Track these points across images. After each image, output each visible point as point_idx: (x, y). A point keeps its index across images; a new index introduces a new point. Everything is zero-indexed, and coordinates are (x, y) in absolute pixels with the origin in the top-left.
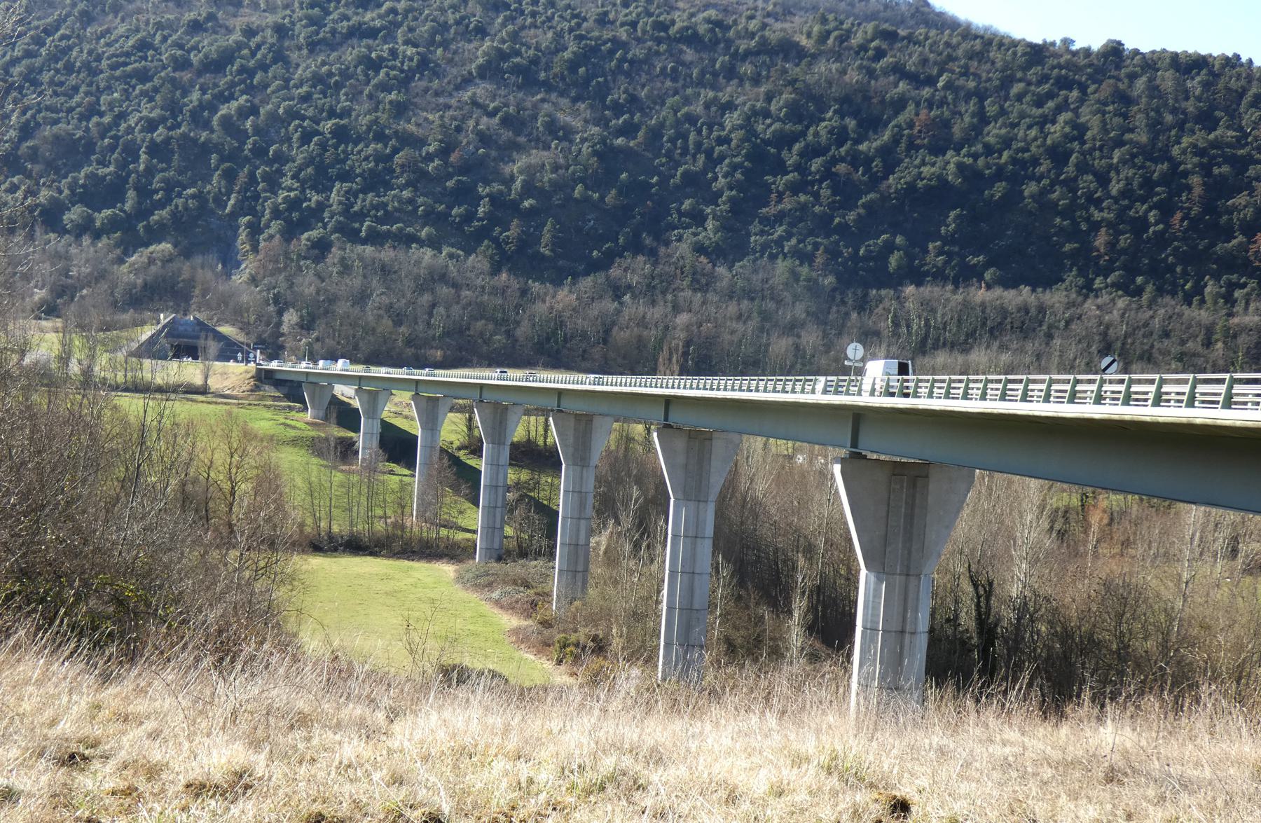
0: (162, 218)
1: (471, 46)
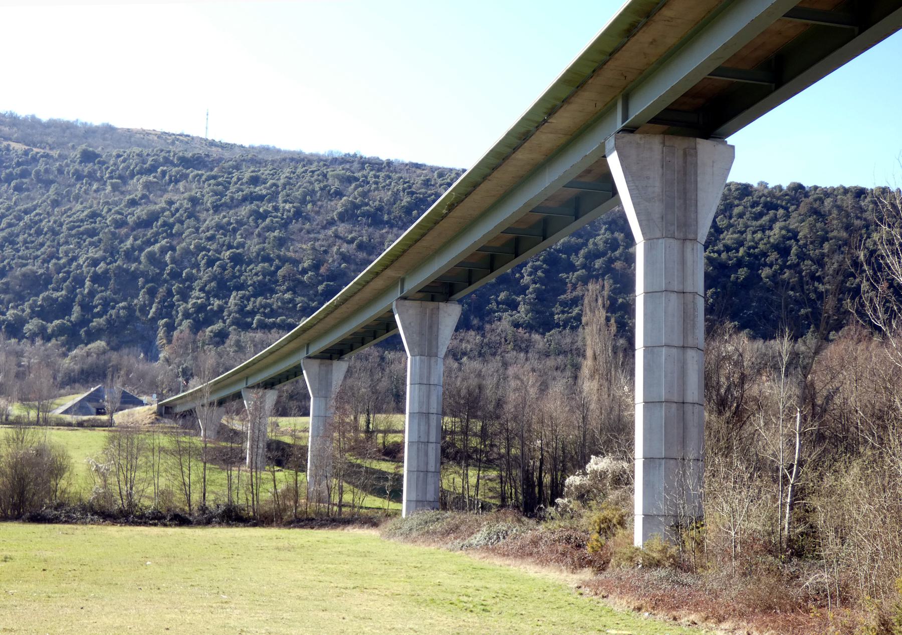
0: (99, 324)
1: (332, 203)
